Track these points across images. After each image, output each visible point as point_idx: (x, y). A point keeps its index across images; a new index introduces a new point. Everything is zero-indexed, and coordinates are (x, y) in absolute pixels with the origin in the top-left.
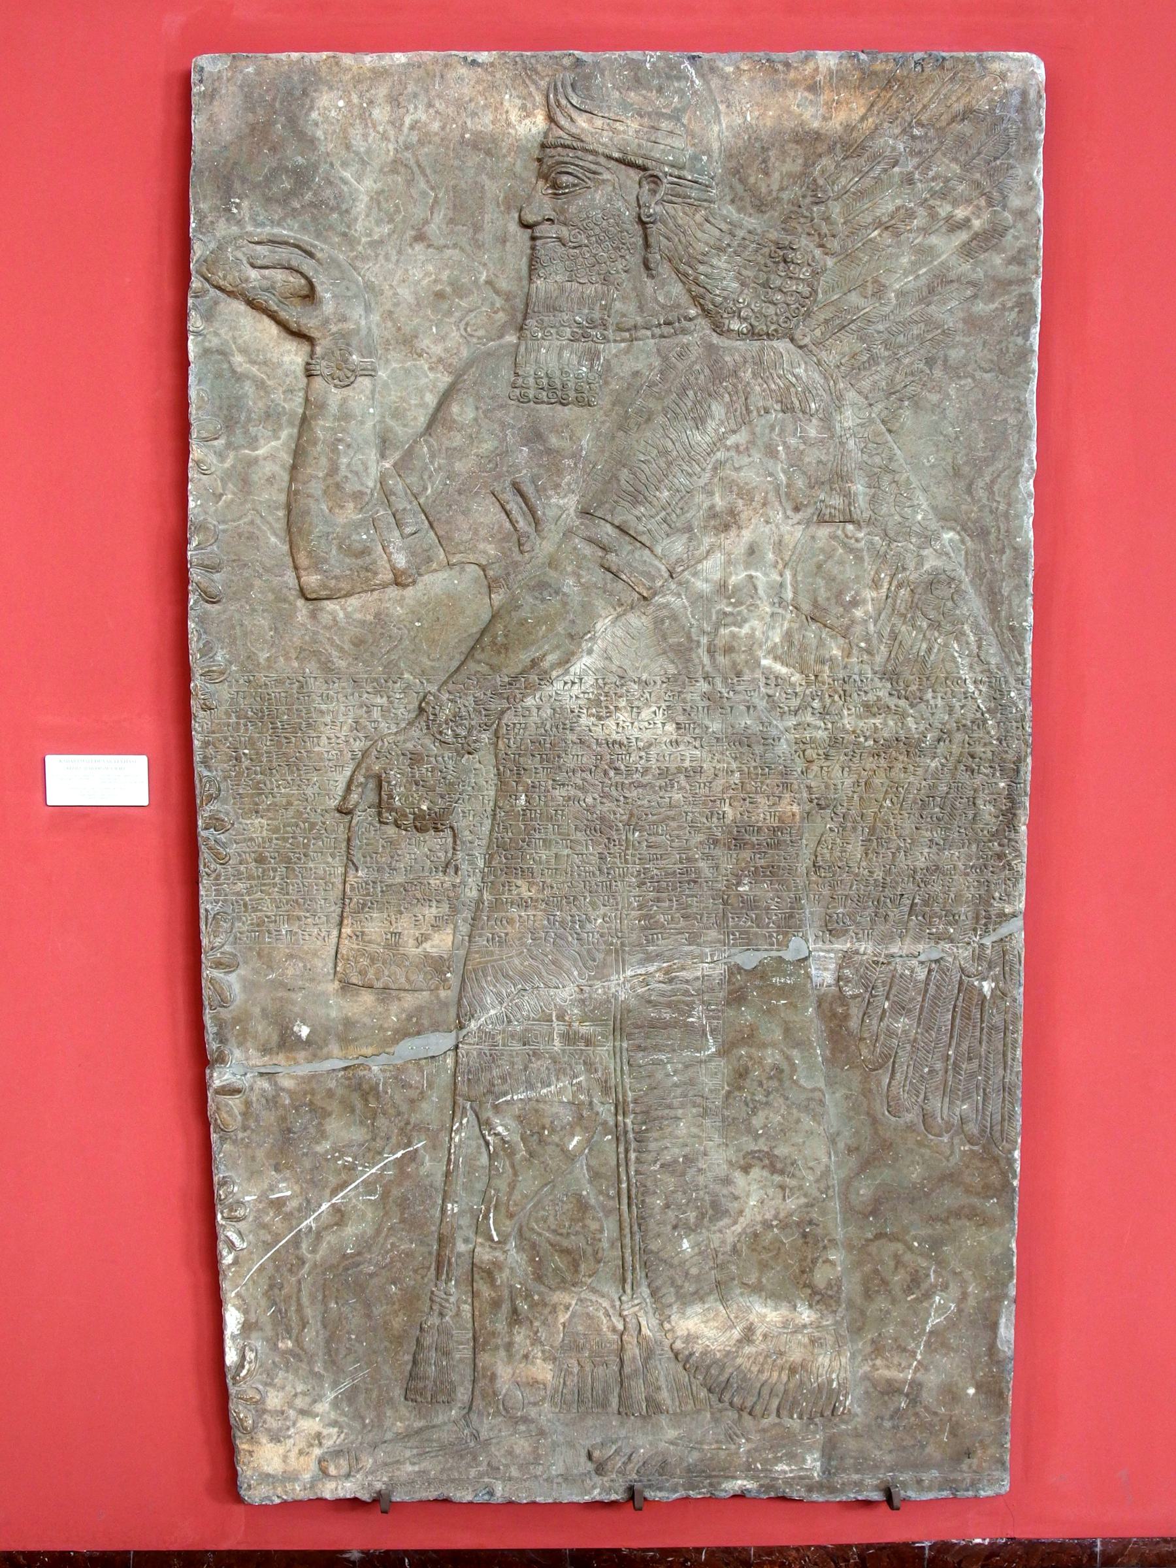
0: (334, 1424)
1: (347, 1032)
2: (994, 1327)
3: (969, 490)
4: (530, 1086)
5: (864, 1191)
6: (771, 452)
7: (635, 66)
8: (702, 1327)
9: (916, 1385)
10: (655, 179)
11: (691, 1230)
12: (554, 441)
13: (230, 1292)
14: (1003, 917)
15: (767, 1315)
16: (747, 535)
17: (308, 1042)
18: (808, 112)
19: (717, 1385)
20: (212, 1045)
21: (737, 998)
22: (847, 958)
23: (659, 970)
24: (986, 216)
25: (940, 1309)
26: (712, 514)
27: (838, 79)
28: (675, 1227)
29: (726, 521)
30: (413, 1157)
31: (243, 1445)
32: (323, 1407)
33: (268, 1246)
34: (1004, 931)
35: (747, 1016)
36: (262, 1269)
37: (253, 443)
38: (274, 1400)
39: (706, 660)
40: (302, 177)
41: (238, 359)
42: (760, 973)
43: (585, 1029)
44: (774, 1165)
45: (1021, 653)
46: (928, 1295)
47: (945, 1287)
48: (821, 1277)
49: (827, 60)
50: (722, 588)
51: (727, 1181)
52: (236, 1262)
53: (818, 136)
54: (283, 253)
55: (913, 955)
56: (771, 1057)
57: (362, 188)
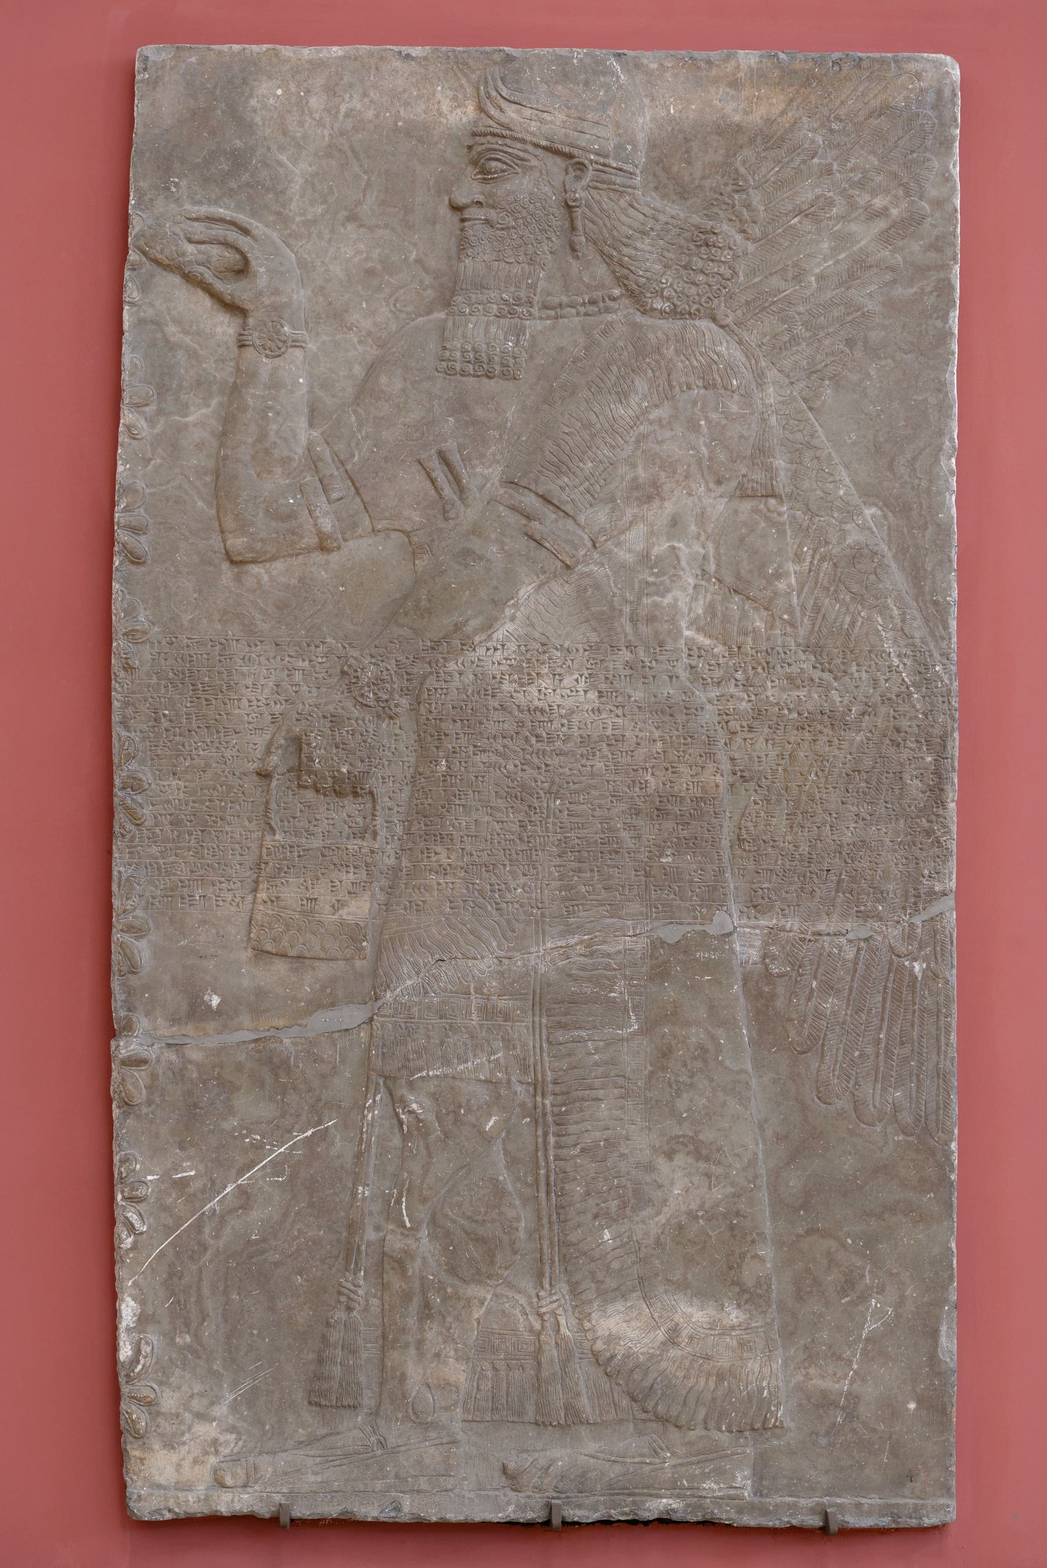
0: (233, 1429)
1: (259, 1003)
2: (935, 1334)
3: (891, 466)
4: (446, 1062)
5: (794, 1182)
6: (693, 426)
7: (565, 61)
8: (624, 1327)
9: (853, 1398)
10: (581, 167)
11: (612, 1220)
12: (479, 412)
13: (127, 1281)
14: (933, 896)
15: (693, 1314)
16: (669, 507)
17: (219, 1012)
18: (730, 107)
19: (641, 1396)
20: (119, 1012)
21: (660, 973)
22: (773, 934)
23: (581, 942)
24: (904, 205)
25: (876, 1313)
26: (635, 485)
27: (758, 76)
28: (596, 1217)
29: (648, 493)
30: (323, 1136)
31: (134, 1451)
32: (221, 1410)
33: (169, 1230)
34: (934, 909)
35: (670, 992)
36: (162, 1255)
37: (184, 409)
38: (169, 1401)
39: (629, 629)
40: (239, 161)
41: (172, 330)
42: (683, 947)
43: (503, 1003)
44: (699, 1151)
45: (946, 627)
46: (863, 1298)
47: (881, 1290)
48: (749, 1274)
49: (748, 59)
50: (644, 558)
51: (650, 1168)
52: (134, 1247)
53: (739, 128)
54: (219, 231)
55: (842, 933)
56: (696, 1035)
57: (298, 170)
